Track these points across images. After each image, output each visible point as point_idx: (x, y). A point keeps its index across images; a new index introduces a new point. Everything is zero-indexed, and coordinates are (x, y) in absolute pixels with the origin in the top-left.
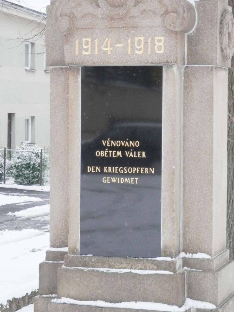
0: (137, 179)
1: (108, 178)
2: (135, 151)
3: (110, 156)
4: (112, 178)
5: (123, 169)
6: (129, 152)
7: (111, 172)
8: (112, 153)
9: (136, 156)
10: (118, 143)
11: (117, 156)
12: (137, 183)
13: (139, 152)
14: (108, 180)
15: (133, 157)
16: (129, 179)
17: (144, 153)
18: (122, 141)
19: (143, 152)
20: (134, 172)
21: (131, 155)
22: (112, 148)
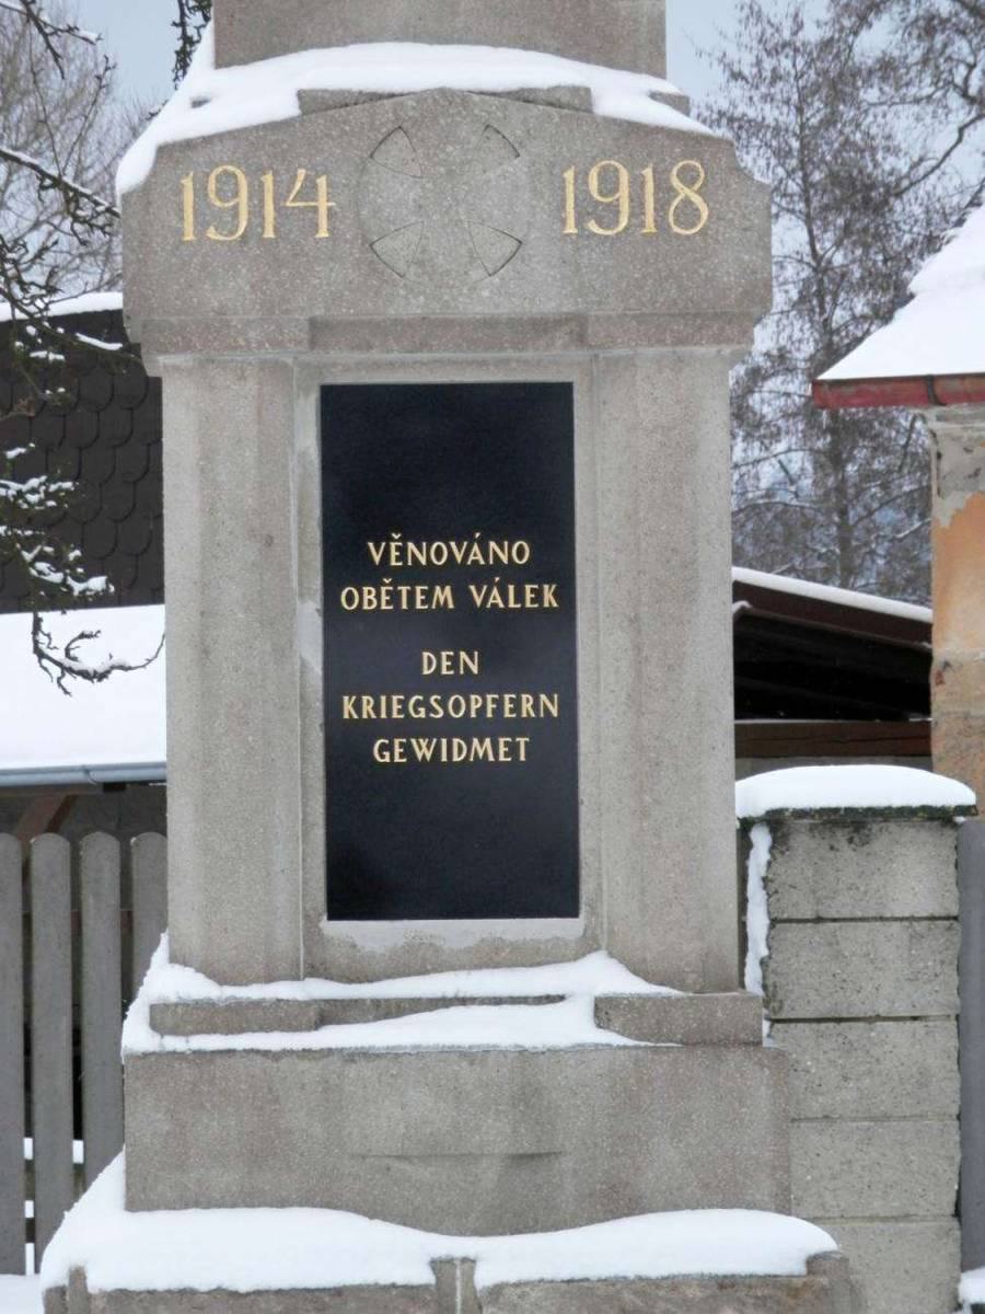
0: (522, 741)
1: (397, 742)
2: (451, 610)
3: (404, 606)
4: (414, 741)
5: (426, 704)
6: (485, 587)
7: (373, 716)
8: (411, 595)
9: (516, 603)
10: (439, 553)
11: (434, 607)
12: (522, 758)
13: (528, 588)
14: (398, 750)
15: (501, 605)
16: (488, 741)
17: (550, 588)
18: (453, 544)
19: (546, 587)
20: (473, 715)
21: (494, 598)
22: (414, 574)
